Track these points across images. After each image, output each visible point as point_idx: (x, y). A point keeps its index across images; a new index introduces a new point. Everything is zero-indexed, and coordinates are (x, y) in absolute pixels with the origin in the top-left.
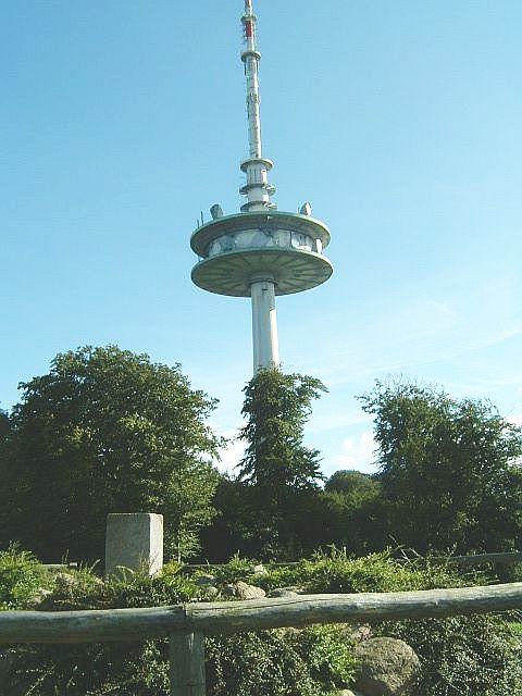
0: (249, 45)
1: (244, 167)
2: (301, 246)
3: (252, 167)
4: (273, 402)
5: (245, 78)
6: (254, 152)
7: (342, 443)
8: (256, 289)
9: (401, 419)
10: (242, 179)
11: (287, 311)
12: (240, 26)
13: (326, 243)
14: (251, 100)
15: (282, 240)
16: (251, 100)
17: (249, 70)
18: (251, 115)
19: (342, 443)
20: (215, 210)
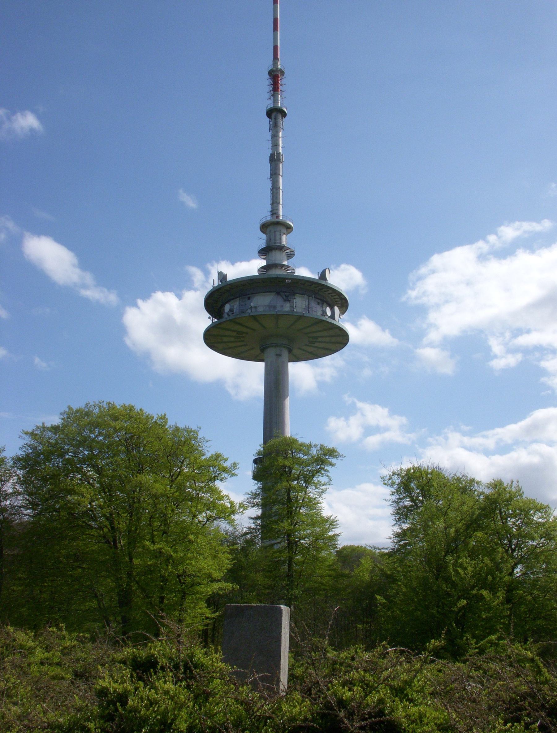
0: (275, 101)
1: (264, 227)
2: (317, 311)
3: (271, 228)
4: (285, 470)
5: (269, 135)
6: (274, 212)
7: (359, 514)
8: (271, 352)
9: (418, 490)
10: (261, 241)
11: (301, 374)
12: (266, 81)
13: (343, 312)
14: (275, 159)
15: (300, 304)
16: (275, 159)
17: (274, 128)
18: (274, 174)
19: (359, 514)
20: (69, 407)
